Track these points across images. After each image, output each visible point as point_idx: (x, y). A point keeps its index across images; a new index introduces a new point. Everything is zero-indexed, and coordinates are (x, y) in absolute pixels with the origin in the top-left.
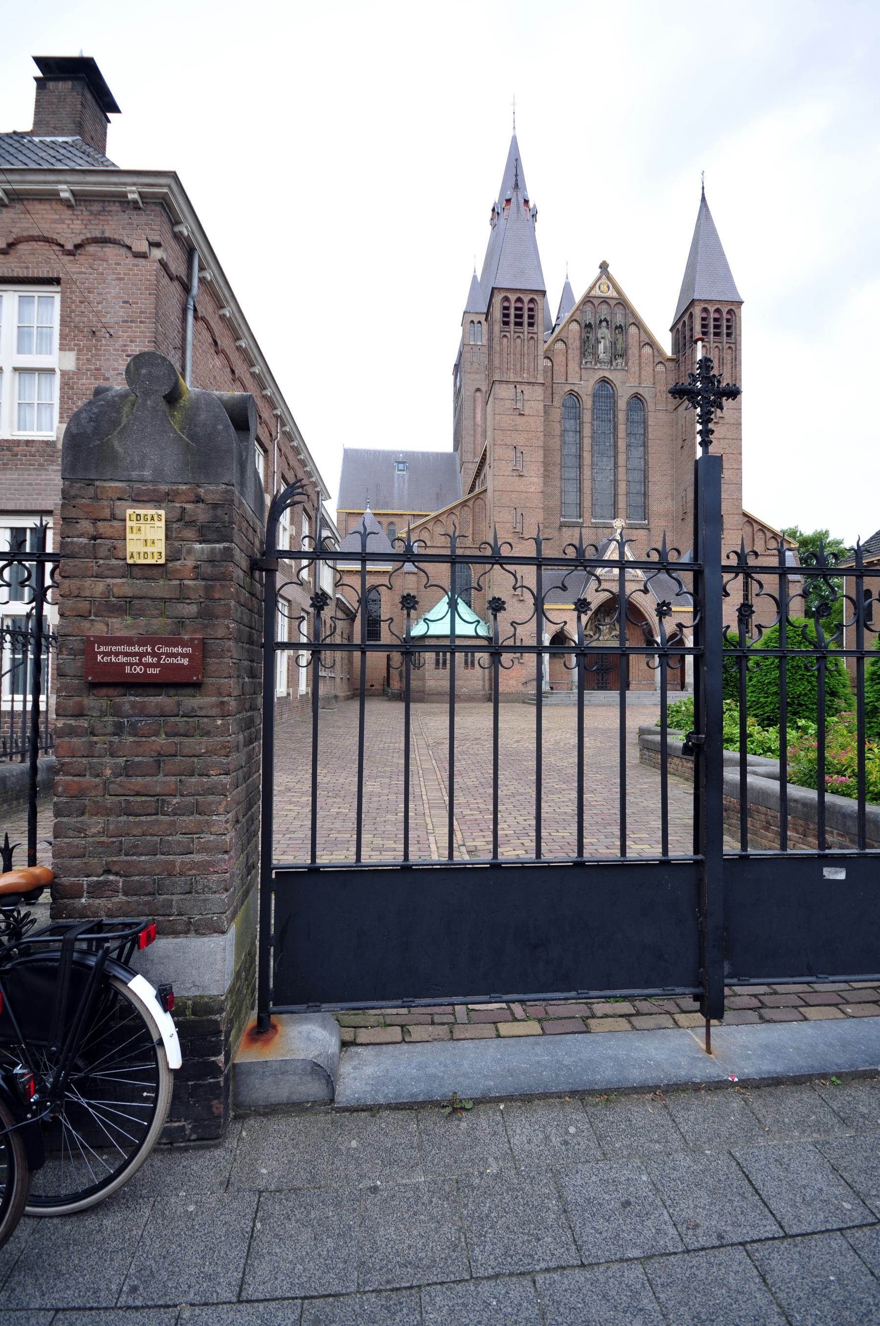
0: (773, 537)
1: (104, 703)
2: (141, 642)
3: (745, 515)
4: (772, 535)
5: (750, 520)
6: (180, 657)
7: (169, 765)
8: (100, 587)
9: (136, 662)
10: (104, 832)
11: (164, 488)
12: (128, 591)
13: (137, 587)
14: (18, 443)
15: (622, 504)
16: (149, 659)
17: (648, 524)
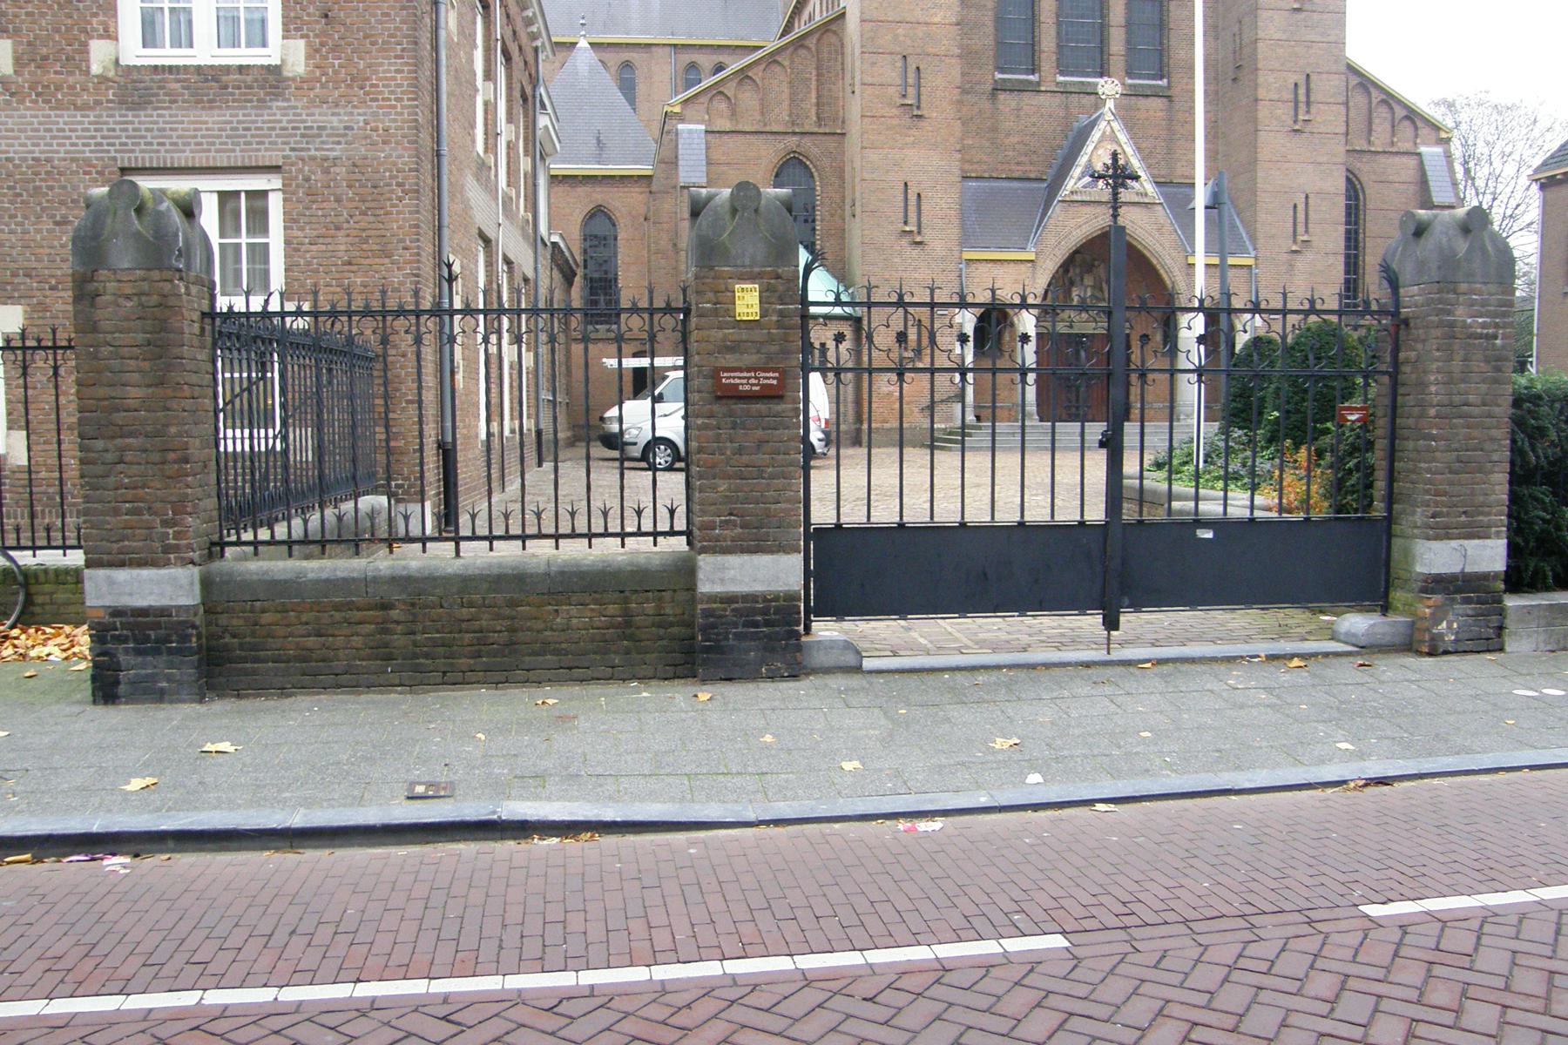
0: (1407, 117)
1: (724, 409)
2: (749, 370)
3: (1352, 69)
4: (1404, 113)
5: (1366, 83)
6: (771, 379)
7: (768, 447)
8: (720, 334)
9: (746, 382)
10: (729, 490)
11: (757, 270)
12: (736, 337)
13: (744, 335)
14: (227, 69)
15: (1117, 44)
16: (753, 381)
17: (1169, 87)
